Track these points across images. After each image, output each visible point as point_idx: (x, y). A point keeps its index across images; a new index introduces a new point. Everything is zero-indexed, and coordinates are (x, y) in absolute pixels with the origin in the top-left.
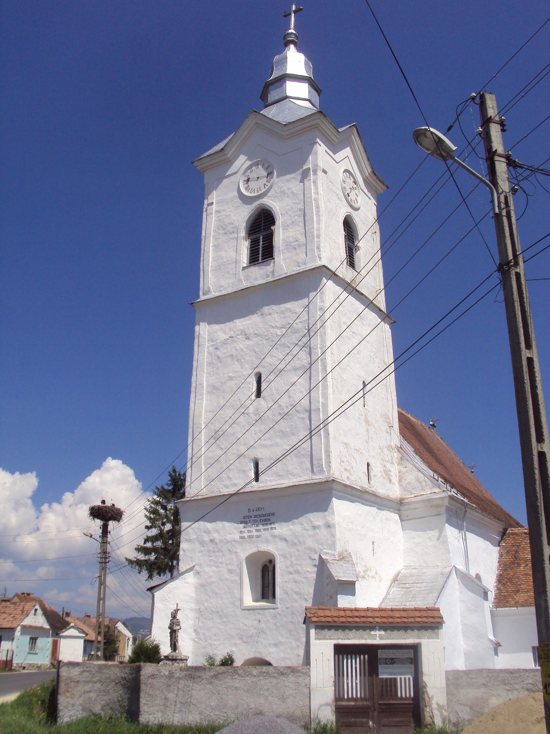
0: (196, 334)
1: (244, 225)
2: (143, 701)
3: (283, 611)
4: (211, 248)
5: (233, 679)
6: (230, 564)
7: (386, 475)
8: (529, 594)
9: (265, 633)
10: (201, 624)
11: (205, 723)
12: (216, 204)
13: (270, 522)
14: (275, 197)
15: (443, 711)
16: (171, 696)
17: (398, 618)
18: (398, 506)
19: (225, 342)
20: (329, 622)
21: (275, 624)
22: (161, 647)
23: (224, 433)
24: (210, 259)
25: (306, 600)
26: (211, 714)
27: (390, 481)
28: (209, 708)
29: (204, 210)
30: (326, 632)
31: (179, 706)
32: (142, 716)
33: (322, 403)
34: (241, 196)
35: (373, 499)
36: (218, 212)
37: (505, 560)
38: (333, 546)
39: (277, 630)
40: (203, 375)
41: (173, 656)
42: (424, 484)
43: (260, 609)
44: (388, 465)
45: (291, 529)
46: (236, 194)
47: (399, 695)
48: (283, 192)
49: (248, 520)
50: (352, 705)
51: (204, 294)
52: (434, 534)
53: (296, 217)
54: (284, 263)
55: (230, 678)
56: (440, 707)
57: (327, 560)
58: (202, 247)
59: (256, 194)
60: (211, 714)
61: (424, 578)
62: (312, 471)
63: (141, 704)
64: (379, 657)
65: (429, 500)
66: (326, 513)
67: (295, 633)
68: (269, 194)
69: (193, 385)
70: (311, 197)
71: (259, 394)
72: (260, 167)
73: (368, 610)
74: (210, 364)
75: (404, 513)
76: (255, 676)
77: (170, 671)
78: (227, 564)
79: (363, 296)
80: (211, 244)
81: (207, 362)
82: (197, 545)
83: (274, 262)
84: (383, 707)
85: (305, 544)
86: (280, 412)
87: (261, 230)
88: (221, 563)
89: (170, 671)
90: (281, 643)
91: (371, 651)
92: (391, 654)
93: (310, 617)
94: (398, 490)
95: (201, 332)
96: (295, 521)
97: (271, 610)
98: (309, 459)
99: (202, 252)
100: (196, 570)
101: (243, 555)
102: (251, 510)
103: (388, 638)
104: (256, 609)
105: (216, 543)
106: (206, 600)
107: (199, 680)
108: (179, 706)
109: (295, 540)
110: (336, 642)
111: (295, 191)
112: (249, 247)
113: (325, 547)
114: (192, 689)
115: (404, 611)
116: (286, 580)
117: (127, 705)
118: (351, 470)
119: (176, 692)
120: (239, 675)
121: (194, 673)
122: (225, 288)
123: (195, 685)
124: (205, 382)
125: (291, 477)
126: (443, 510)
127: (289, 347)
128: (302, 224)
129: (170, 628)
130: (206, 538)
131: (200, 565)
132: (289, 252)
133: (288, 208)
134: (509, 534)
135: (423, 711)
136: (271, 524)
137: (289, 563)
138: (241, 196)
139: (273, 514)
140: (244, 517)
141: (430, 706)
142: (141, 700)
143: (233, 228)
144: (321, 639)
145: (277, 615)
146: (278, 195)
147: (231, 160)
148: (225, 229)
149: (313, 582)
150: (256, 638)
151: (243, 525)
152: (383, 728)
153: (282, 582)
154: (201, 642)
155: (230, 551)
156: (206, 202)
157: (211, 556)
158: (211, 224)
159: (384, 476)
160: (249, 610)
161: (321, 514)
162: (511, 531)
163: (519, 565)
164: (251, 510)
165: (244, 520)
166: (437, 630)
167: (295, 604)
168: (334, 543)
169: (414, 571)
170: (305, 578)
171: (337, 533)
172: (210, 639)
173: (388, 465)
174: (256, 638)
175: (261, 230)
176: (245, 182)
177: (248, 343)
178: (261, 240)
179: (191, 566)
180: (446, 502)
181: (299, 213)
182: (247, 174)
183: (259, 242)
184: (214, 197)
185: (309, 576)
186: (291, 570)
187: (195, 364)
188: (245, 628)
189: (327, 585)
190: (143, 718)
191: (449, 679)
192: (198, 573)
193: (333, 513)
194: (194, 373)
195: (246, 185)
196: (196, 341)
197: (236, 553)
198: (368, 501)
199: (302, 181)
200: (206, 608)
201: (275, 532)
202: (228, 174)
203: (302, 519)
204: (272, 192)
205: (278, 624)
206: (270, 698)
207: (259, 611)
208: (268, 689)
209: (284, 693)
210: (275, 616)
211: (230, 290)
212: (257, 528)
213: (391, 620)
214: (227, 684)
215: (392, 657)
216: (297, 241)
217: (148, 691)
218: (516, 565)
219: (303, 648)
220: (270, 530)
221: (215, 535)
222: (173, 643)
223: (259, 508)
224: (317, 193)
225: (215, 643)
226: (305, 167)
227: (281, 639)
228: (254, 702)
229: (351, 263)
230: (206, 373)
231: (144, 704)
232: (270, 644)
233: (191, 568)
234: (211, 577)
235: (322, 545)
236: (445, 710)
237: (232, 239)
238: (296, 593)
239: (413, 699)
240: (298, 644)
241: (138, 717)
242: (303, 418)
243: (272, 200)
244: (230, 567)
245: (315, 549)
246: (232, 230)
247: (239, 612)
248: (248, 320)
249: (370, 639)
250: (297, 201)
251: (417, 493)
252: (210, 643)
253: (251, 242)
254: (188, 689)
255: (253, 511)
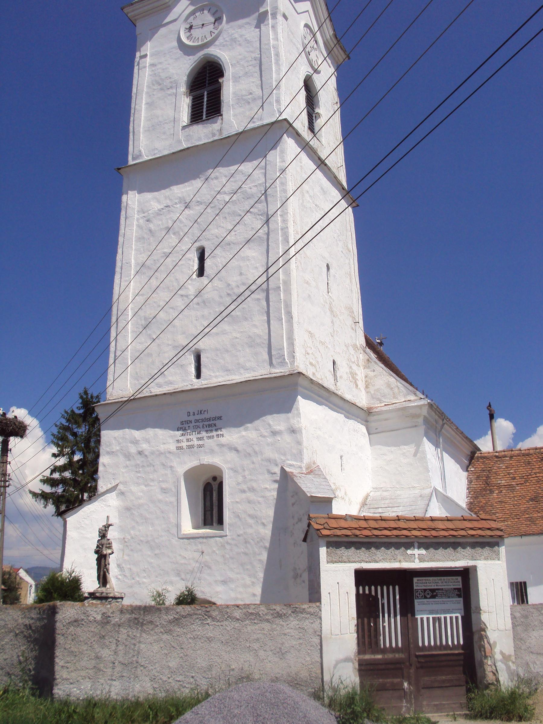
0: (124, 205)
1: (185, 78)
2: (59, 662)
3: (233, 539)
4: (143, 106)
5: (203, 625)
6: (163, 481)
7: (353, 377)
8: (506, 523)
9: (210, 568)
10: (126, 558)
11: (162, 695)
12: (151, 56)
13: (215, 428)
14: (224, 46)
15: (510, 663)
16: (106, 653)
17: (443, 530)
18: (365, 415)
19: (159, 213)
20: (347, 536)
21: (223, 556)
22: (83, 580)
23: (157, 320)
24: (143, 118)
25: (264, 524)
26: (170, 680)
27: (357, 386)
28: (167, 671)
29: (136, 64)
30: (342, 552)
31: (118, 668)
32: (59, 687)
33: (283, 280)
34: (181, 45)
35: (340, 403)
36: (152, 65)
37: (475, 486)
38: (299, 456)
39: (225, 564)
40: (131, 252)
41: (102, 593)
42: (396, 390)
43: (203, 537)
44: (355, 367)
45: (243, 436)
46: (175, 44)
47: (420, 644)
48: (234, 40)
49: (186, 426)
50: (379, 659)
51: (134, 159)
52: (410, 449)
53: (250, 68)
54: (234, 118)
55: (199, 623)
56: (506, 658)
57: (292, 473)
58: (133, 105)
59: (200, 43)
60: (170, 680)
61: (399, 501)
62: (271, 364)
63: (57, 668)
64: (415, 588)
65: (404, 409)
66: (290, 415)
67: (249, 567)
68: (217, 43)
69: (118, 264)
70: (269, 44)
71: (201, 272)
72: (206, 12)
73: (399, 520)
74: (140, 239)
75: (373, 425)
76: (238, 619)
77: (103, 614)
78: (160, 482)
79: (325, 167)
80: (144, 102)
81: (136, 236)
82: (121, 458)
83: (222, 119)
84: (422, 660)
85: (262, 453)
86: (229, 292)
87: (206, 87)
88: (153, 480)
89: (103, 614)
90: (231, 580)
91: (403, 579)
92: (431, 583)
93: (318, 530)
94: (364, 398)
95: (129, 202)
96: (249, 425)
97: (218, 539)
98: (266, 350)
99: (132, 111)
100: (120, 490)
101: (181, 470)
102: (192, 414)
103: (431, 560)
104: (198, 538)
105: (146, 456)
106: (133, 528)
107: (151, 627)
108: (118, 668)
109: (249, 450)
110: (358, 566)
111: (249, 39)
112: (190, 105)
113: (289, 457)
114: (140, 642)
115: (448, 520)
116: (238, 500)
117: (34, 669)
118: (317, 364)
119: (113, 647)
120: (214, 619)
121: (141, 616)
122: (160, 151)
123: (144, 635)
124: (133, 261)
125: (242, 371)
126: (421, 420)
127: (240, 215)
128: (257, 75)
129: (96, 552)
130: (133, 450)
131: (125, 483)
132: (240, 107)
133: (240, 57)
134: (478, 457)
135: (482, 664)
136: (216, 430)
137: (240, 479)
138: (181, 45)
139: (220, 418)
140: (182, 423)
141: (492, 657)
142: (57, 660)
143: (171, 82)
144: (336, 562)
145: (226, 545)
146: (228, 43)
147: (169, 6)
148: (161, 84)
149: (272, 502)
150: (198, 574)
151: (180, 432)
152: (423, 691)
153: (232, 502)
154: (126, 580)
155: (163, 465)
156: (138, 55)
157: (139, 472)
158: (143, 78)
159: (351, 378)
160: (188, 538)
161: (283, 416)
162: (480, 455)
163: (492, 492)
164: (192, 414)
165: (182, 426)
166: (497, 547)
167: (250, 531)
168: (301, 453)
169: (385, 494)
170: (263, 497)
171: (304, 439)
172: (139, 576)
173: (355, 367)
174: (198, 574)
175: (205, 85)
176: (187, 31)
177: (189, 213)
178: (205, 97)
179: (113, 485)
180: (425, 411)
181: (254, 62)
182: (189, 21)
183: (203, 99)
184: (148, 48)
185: (268, 494)
186: (244, 487)
187: (121, 239)
188: (183, 561)
189: (293, 504)
190: (60, 691)
191: (515, 617)
192: (122, 493)
193: (299, 415)
194: (120, 251)
195: (188, 34)
196: (123, 213)
197: (171, 467)
198: (334, 405)
199: (258, 26)
200: (132, 538)
201: (222, 440)
202: (166, 21)
203: (257, 423)
204: (220, 40)
205: (228, 556)
206: (261, 653)
207: (201, 540)
208: (258, 640)
209: (283, 644)
210: (223, 546)
211: (166, 153)
212: (199, 436)
213: (434, 533)
214: (194, 633)
215: (433, 587)
216: (251, 94)
217: (67, 646)
218: (488, 492)
219: (261, 585)
220: (216, 438)
221: (144, 446)
222: (102, 573)
223: (202, 411)
224: (276, 39)
225: (144, 580)
226: (262, 10)
227: (231, 575)
228: (239, 660)
229: (311, 128)
230: (136, 250)
231: (62, 667)
232: (216, 581)
233: (114, 487)
234: (139, 498)
235: (284, 454)
236: (513, 662)
237: (170, 95)
238: (250, 516)
239: (463, 647)
240: (253, 580)
241: (52, 689)
242: (258, 300)
243: (220, 49)
244: (164, 485)
245: (275, 460)
246: (169, 85)
247: (175, 541)
248: (189, 186)
249: (407, 561)
250: (252, 49)
251: (387, 401)
252: (138, 581)
253: (193, 99)
254: (133, 641)
255: (194, 414)
